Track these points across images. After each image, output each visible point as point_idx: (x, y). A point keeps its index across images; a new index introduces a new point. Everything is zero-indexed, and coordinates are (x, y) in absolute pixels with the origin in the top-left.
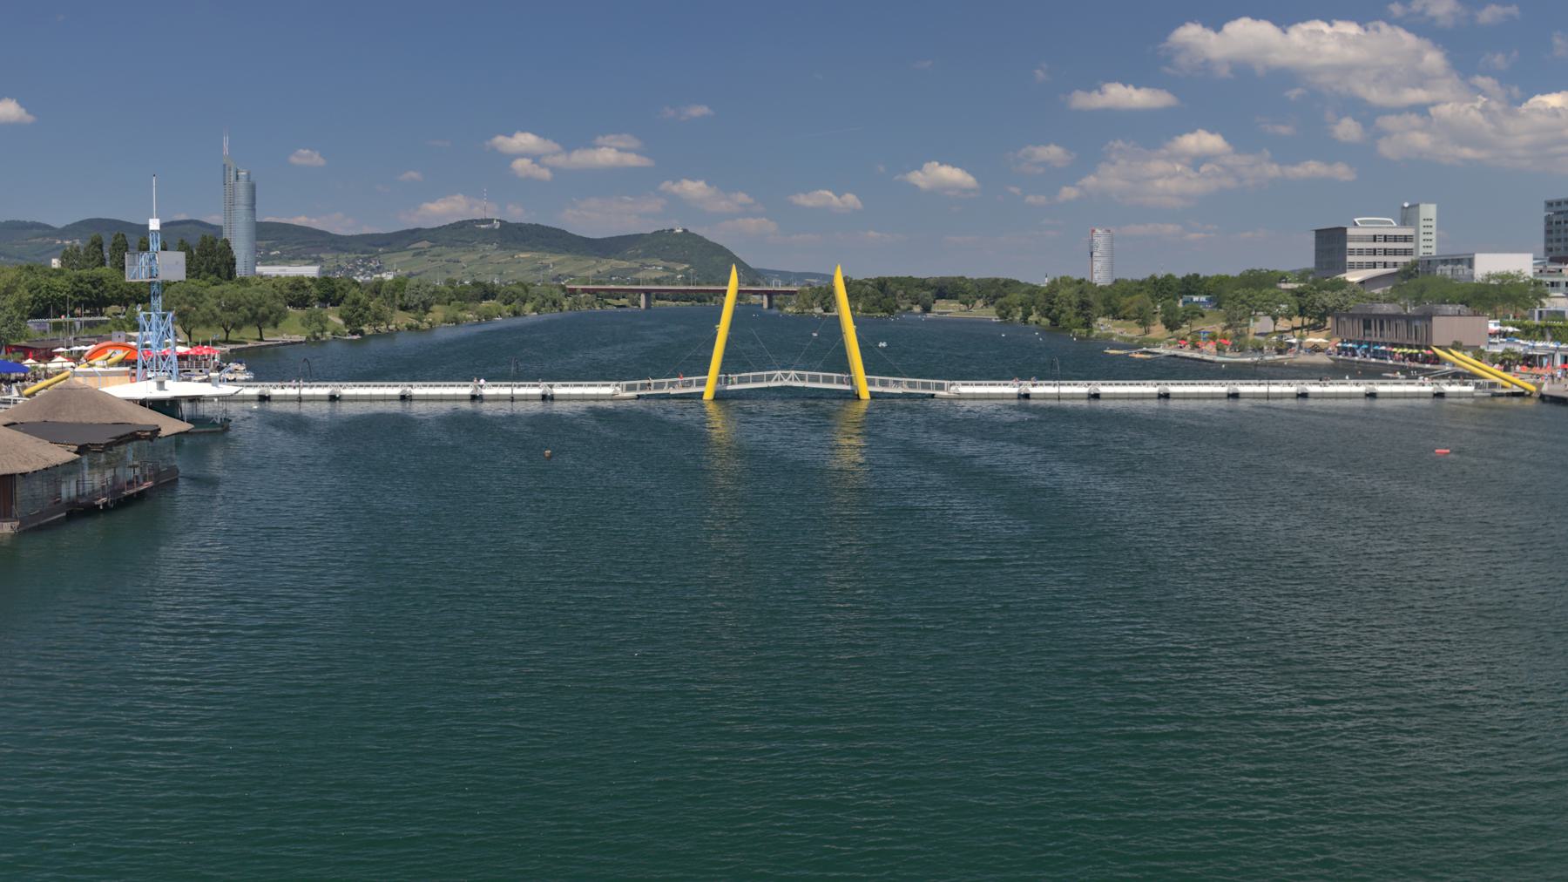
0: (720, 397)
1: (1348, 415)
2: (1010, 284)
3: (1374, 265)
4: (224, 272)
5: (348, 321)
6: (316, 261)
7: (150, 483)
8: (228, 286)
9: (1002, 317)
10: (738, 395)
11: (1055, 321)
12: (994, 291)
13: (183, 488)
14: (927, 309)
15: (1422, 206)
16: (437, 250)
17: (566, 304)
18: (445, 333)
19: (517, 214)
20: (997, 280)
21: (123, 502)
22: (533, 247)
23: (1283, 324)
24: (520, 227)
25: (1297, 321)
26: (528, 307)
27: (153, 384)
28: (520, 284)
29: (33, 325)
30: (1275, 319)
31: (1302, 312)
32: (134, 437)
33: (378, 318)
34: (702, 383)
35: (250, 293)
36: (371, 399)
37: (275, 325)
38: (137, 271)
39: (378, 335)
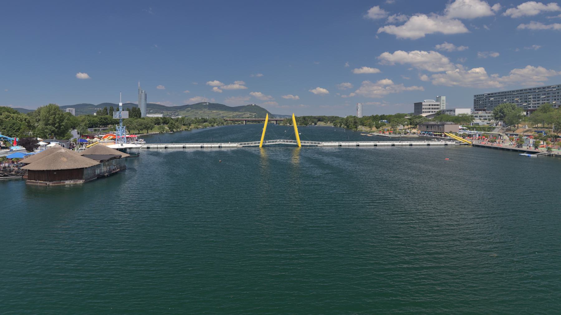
0: (263, 146)
2: (337, 118)
3: (429, 112)
5: (170, 128)
6: (162, 113)
10: (268, 146)
11: (348, 127)
12: (333, 119)
17: (225, 123)
18: (194, 131)
19: (213, 101)
21: (112, 174)
22: (217, 109)
23: (406, 127)
24: (213, 104)
25: (410, 126)
26: (215, 124)
27: (120, 145)
29: (89, 130)
30: (404, 126)
31: (411, 124)
32: (115, 158)
33: (178, 127)
35: (145, 121)
38: (116, 116)
39: (177, 132)
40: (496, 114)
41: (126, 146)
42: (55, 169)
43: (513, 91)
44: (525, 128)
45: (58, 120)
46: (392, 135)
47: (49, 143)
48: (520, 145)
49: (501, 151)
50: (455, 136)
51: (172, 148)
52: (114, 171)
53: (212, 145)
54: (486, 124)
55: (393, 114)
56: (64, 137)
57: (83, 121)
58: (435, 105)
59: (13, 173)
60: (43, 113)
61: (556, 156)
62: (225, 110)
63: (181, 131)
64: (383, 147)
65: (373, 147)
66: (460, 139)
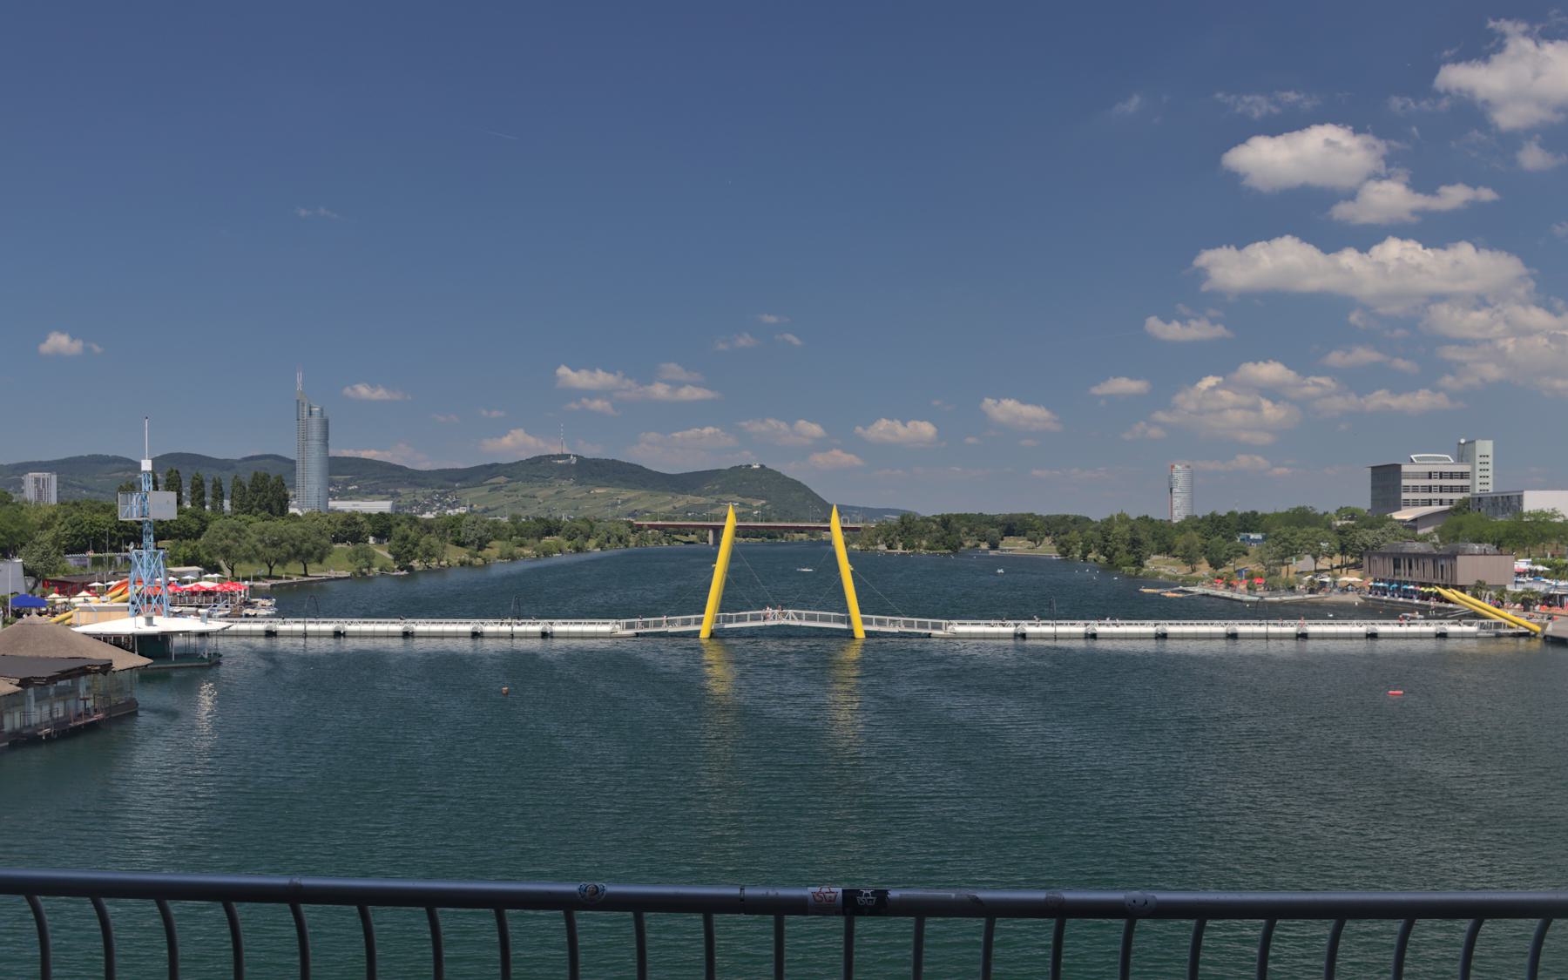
0: (712, 635)
2: (1078, 521)
3: (1430, 503)
4: (276, 508)
5: (397, 557)
6: (394, 495)
7: (101, 716)
8: (279, 525)
9: (1063, 554)
10: (738, 633)
11: (1110, 556)
12: (1057, 527)
13: (144, 719)
14: (994, 546)
15: (1479, 443)
16: (513, 485)
18: (500, 569)
19: (592, 450)
20: (1066, 517)
21: (65, 733)
22: (609, 483)
23: (1324, 563)
24: (596, 463)
25: (1337, 560)
26: (591, 544)
27: (141, 620)
28: (585, 520)
29: (71, 561)
30: (1315, 557)
31: (1343, 550)
32: (84, 671)
33: (428, 554)
34: (699, 622)
37: (320, 561)
38: (130, 510)
41: (163, 624)
46: (1262, 595)
55: (1282, 509)
57: (45, 526)
58: (1451, 476)
62: (644, 486)
63: (441, 570)
64: (1193, 647)
65: (1082, 644)
66: (1510, 616)
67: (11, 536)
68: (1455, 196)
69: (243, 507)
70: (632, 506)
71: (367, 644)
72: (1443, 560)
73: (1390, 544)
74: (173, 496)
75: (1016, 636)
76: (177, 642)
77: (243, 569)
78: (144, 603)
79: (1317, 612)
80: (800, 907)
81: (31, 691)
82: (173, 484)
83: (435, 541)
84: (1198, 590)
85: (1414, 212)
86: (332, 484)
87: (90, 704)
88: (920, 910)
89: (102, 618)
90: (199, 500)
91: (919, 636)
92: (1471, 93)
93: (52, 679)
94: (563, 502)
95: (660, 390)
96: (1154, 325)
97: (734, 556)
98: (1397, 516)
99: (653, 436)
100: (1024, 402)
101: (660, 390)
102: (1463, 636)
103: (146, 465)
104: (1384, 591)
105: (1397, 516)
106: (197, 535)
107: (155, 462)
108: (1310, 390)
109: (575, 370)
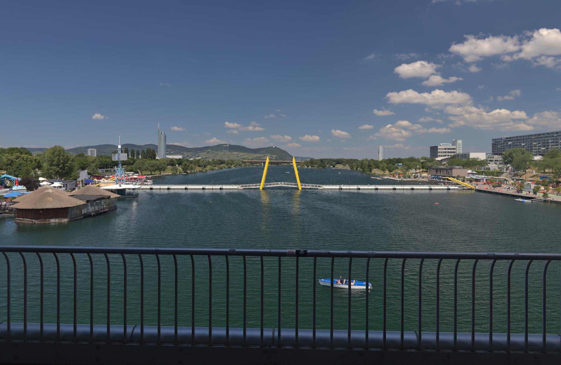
0: (263, 189)
1: (443, 195)
3: (445, 156)
5: (183, 170)
6: (183, 154)
8: (154, 161)
11: (363, 169)
12: (350, 162)
14: (334, 167)
15: (458, 141)
17: (243, 165)
18: (210, 172)
19: (233, 143)
21: (98, 214)
22: (237, 151)
23: (418, 171)
24: (234, 146)
25: (421, 170)
26: (233, 166)
29: (100, 171)
30: (416, 169)
31: (423, 168)
32: (103, 198)
33: (191, 169)
34: (260, 185)
35: (158, 163)
36: (230, 189)
38: (115, 158)
39: (191, 173)
40: (505, 159)
41: (124, 186)
42: (40, 208)
43: (531, 136)
44: (532, 173)
45: (62, 161)
46: (402, 179)
47: (53, 183)
48: (520, 191)
49: (500, 196)
50: (461, 182)
51: (174, 189)
52: (103, 211)
53: (214, 187)
54: (497, 169)
55: (407, 157)
56: (71, 177)
57: (93, 162)
58: (451, 149)
59: (7, 211)
60: (47, 154)
61: (551, 202)
66: (467, 184)
67: (84, 164)
68: (453, 79)
69: (144, 157)
70: (243, 157)
71: (176, 191)
72: (448, 170)
73: (435, 166)
74: (126, 154)
75: (339, 189)
76: (127, 191)
77: (144, 173)
78: (119, 181)
79: (417, 183)
80: (285, 255)
81: (89, 204)
82: (127, 151)
83: (193, 165)
84: (386, 177)
85: (443, 83)
86: (167, 151)
87: (105, 207)
88: (315, 255)
89: (108, 185)
90: (133, 155)
91: (315, 189)
92: (459, 53)
93: (95, 201)
94: (226, 156)
95: (250, 128)
96: (376, 111)
97: (268, 169)
98: (437, 159)
99: (249, 139)
100: (342, 131)
101: (250, 128)
102: (454, 189)
103: (119, 147)
104: (434, 178)
105: (437, 159)
106: (133, 164)
107: (122, 146)
108: (415, 128)
109: (229, 123)
